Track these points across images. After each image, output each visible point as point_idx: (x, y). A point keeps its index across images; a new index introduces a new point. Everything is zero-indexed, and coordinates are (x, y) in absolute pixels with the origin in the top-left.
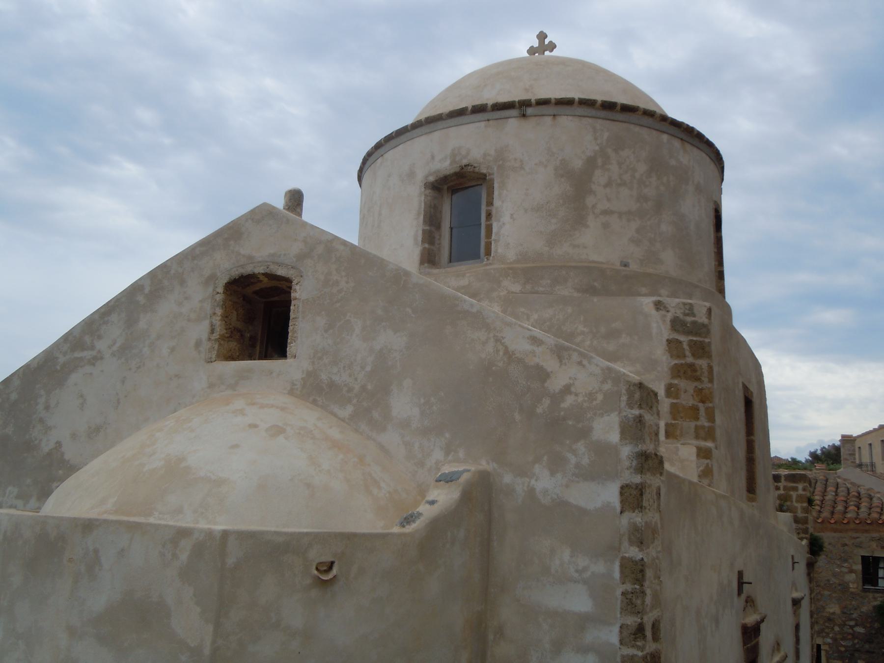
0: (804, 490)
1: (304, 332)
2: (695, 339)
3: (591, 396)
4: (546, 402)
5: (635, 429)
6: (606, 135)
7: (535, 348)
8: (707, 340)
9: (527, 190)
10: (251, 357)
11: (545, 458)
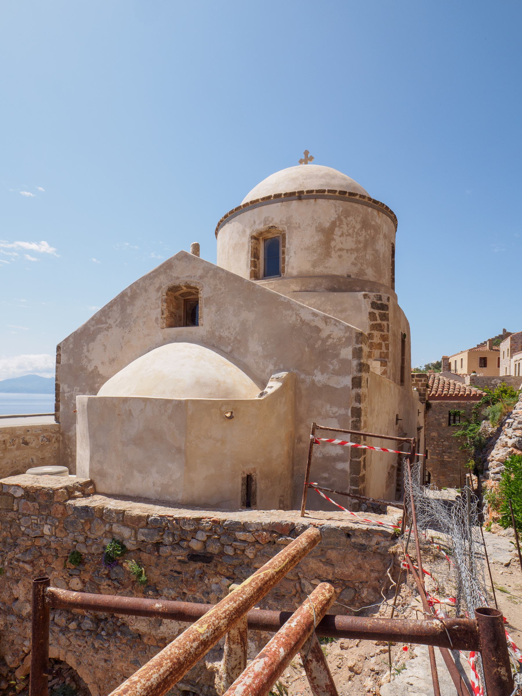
0: (425, 381)
1: (205, 314)
2: (382, 312)
3: (340, 339)
4: (320, 342)
5: (358, 353)
6: (341, 209)
7: (314, 318)
8: (387, 312)
9: (302, 239)
10: (180, 326)
11: (319, 367)
